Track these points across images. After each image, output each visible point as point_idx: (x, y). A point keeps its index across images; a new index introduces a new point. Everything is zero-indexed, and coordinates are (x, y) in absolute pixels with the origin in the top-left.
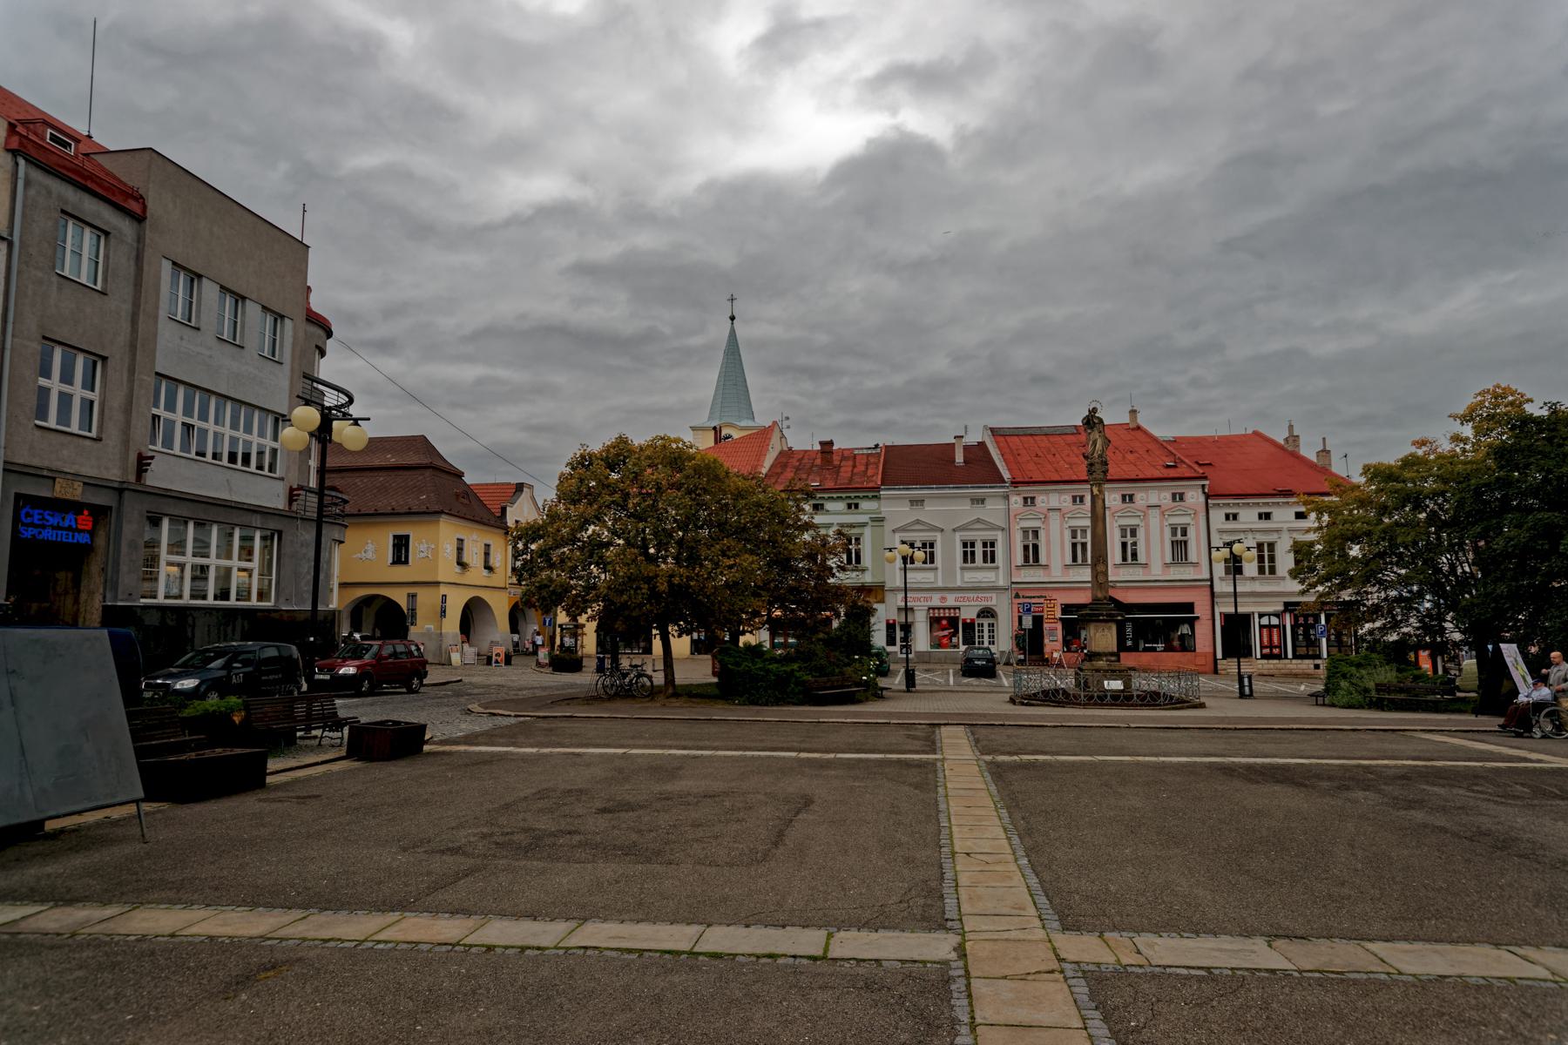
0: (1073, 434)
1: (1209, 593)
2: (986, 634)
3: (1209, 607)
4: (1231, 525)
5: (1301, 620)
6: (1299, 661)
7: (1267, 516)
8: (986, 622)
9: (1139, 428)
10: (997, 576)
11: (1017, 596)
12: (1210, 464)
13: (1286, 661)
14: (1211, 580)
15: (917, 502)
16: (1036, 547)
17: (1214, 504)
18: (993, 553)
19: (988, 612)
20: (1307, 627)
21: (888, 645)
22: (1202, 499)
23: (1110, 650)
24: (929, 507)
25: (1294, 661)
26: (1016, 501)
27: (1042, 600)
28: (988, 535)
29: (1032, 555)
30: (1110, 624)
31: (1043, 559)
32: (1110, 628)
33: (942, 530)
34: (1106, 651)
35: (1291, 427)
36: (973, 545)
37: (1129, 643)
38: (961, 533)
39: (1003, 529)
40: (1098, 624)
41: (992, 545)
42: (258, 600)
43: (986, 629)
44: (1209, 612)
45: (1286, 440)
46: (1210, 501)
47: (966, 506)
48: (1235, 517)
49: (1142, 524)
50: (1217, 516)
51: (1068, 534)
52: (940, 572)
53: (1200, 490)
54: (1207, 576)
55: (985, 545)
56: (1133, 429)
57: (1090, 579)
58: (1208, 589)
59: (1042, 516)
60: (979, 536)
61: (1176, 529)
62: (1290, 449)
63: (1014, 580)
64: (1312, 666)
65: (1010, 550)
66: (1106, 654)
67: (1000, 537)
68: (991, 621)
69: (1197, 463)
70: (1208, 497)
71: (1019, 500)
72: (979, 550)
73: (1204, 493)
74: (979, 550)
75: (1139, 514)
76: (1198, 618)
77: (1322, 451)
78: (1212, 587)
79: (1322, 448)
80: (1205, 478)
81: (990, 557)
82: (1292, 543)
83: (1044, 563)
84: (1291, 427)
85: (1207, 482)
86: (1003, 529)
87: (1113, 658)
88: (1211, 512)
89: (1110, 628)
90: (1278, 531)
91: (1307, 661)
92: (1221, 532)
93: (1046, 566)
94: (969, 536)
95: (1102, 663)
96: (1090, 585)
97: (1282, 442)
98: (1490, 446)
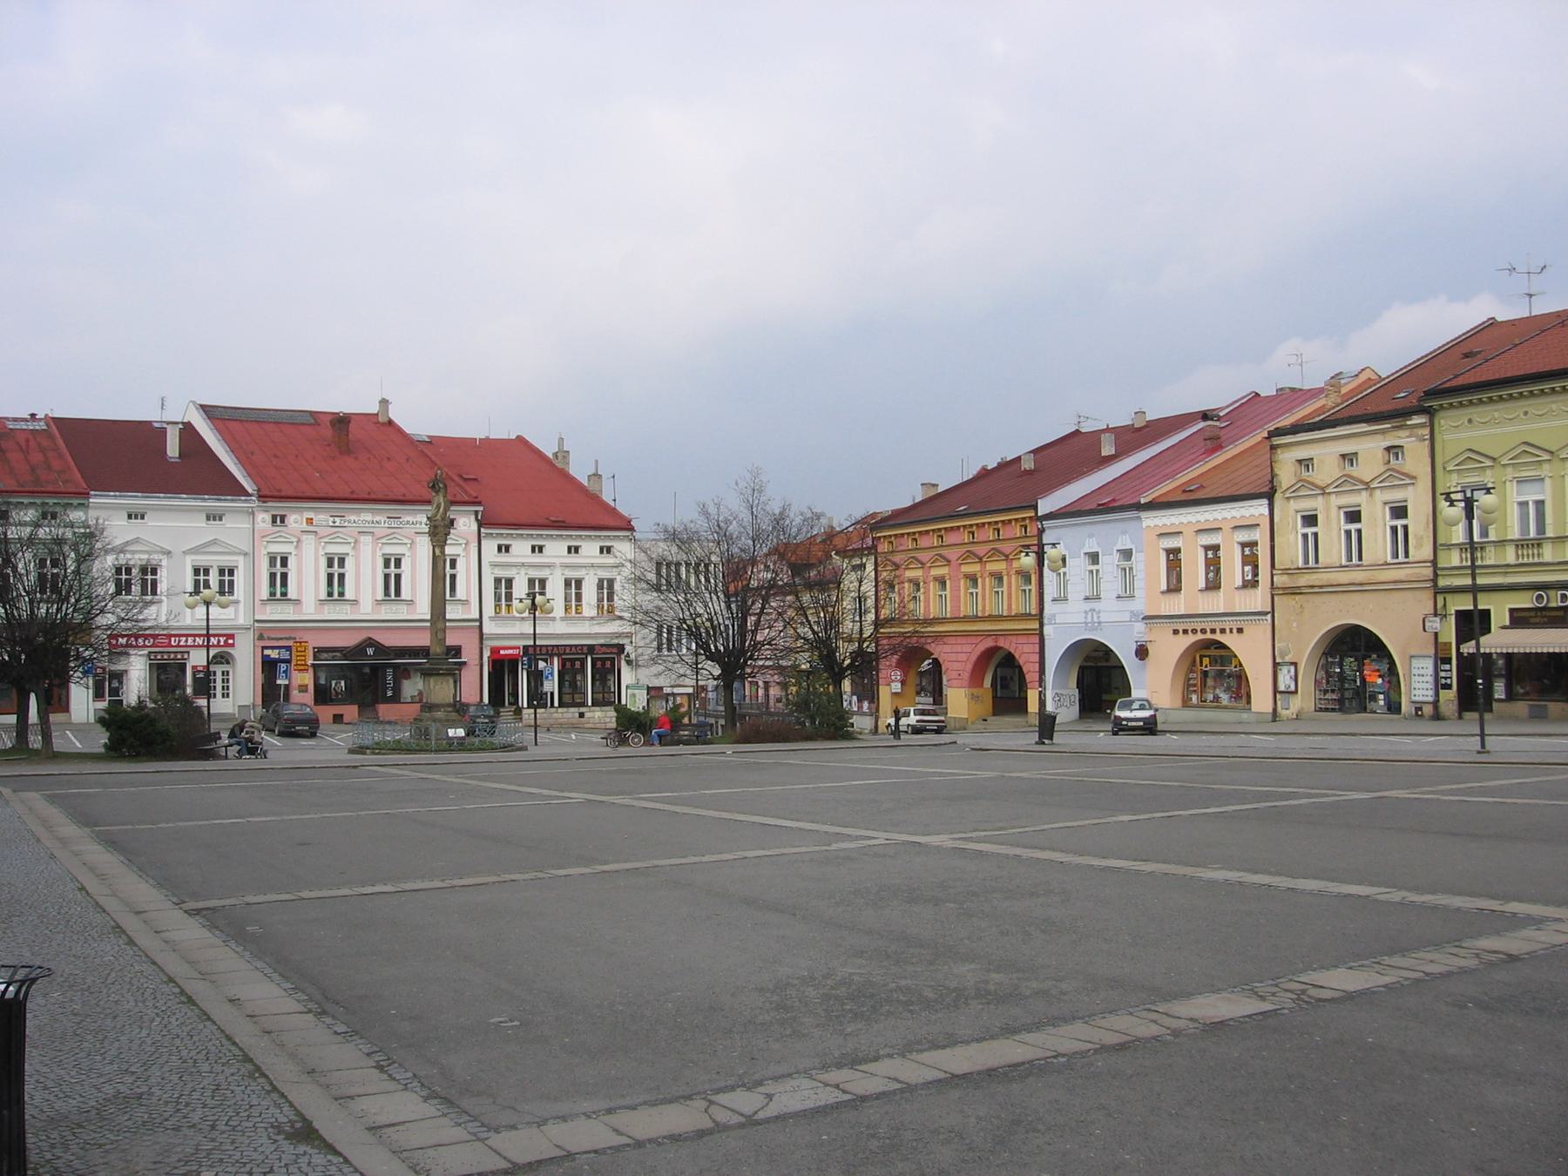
0: (311, 425)
1: (477, 636)
2: (219, 685)
3: (478, 651)
4: (504, 558)
5: (568, 665)
6: (565, 710)
7: (609, 550)
8: (218, 669)
9: (390, 422)
10: (236, 611)
11: (261, 638)
12: (475, 480)
13: (553, 710)
14: (480, 620)
15: (213, 517)
17: (486, 534)
18: (231, 583)
19: (222, 657)
20: (575, 673)
21: (315, 704)
22: (474, 526)
23: (447, 702)
24: (152, 521)
25: (560, 710)
26: (263, 519)
27: (290, 643)
28: (226, 560)
29: (279, 582)
30: (447, 678)
31: (292, 592)
32: (447, 682)
33: (170, 552)
34: (443, 702)
35: (561, 440)
36: (206, 572)
37: (390, 693)
38: (194, 557)
39: (246, 554)
40: (438, 677)
41: (231, 572)
42: (1562, 602)
43: (219, 678)
44: (478, 657)
45: (556, 455)
46: (482, 530)
47: (200, 522)
48: (507, 548)
49: (407, 554)
50: (490, 547)
51: (323, 562)
52: (241, 605)
53: (473, 517)
54: (477, 616)
55: (222, 572)
56: (383, 424)
57: (429, 617)
58: (478, 631)
59: (295, 540)
60: (214, 561)
61: (275, 558)
62: (560, 465)
63: (256, 618)
64: (577, 715)
65: (251, 582)
66: (443, 706)
67: (241, 563)
68: (225, 667)
69: (461, 476)
70: (480, 525)
71: (268, 518)
72: (214, 578)
73: (477, 519)
74: (214, 578)
75: (406, 541)
76: (465, 663)
77: (594, 475)
78: (481, 627)
79: (593, 471)
80: (479, 503)
81: (226, 588)
82: (597, 581)
83: (293, 598)
84: (561, 440)
85: (481, 508)
86: (246, 554)
87: (450, 709)
88: (482, 542)
89: (447, 682)
90: (549, 566)
91: (572, 710)
92: (494, 565)
93: (297, 602)
94: (202, 560)
95: (440, 714)
96: (428, 624)
97: (551, 456)
98: (316, 515)
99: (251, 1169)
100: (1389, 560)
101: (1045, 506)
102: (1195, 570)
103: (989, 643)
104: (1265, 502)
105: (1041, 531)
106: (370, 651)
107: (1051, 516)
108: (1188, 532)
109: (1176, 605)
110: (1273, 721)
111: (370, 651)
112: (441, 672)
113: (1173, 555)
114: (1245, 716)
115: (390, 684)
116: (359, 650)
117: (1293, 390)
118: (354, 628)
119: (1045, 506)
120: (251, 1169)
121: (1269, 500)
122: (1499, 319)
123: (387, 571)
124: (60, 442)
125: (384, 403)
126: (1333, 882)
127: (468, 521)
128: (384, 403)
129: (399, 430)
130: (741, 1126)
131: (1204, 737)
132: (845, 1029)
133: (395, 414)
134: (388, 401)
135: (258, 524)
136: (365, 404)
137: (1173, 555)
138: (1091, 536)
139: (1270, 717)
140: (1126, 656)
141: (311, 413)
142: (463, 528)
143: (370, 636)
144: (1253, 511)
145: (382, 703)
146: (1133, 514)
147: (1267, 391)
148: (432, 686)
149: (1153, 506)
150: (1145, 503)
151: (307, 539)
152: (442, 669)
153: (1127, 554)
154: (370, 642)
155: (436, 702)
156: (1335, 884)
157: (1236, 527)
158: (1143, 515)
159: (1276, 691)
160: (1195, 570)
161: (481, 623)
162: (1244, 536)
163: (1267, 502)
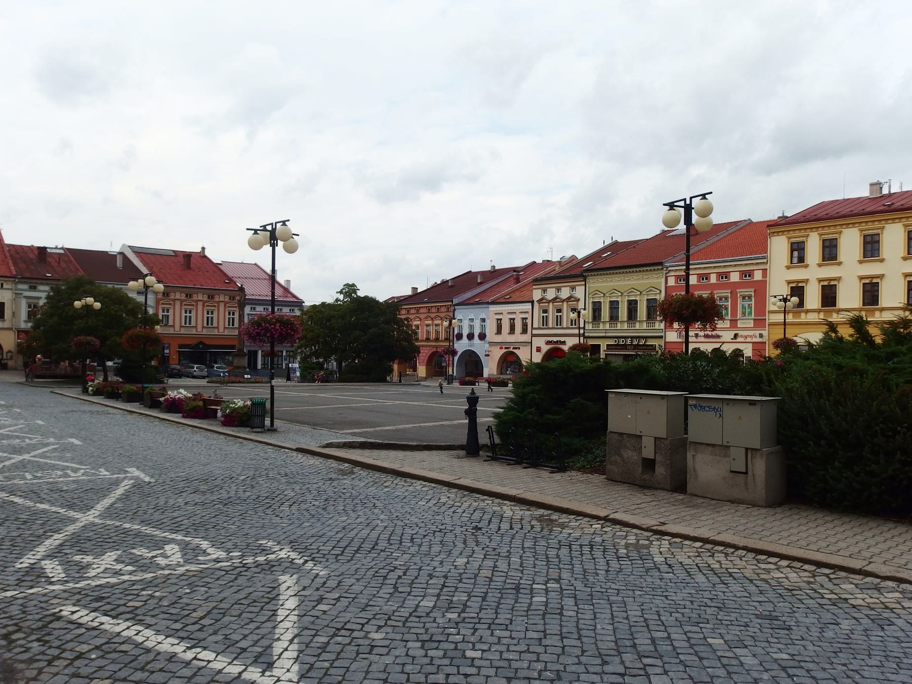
9: (205, 257)
92: (248, 315)
99: (473, 634)
100: (542, 327)
101: (455, 301)
102: (506, 327)
103: (435, 350)
104: (530, 304)
105: (454, 310)
106: (201, 346)
107: (458, 305)
109: (498, 339)
111: (201, 346)
113: (499, 321)
116: (197, 345)
117: (548, 261)
118: (222, 338)
119: (455, 301)
120: (473, 634)
122: (754, 220)
124: (72, 258)
125: (203, 249)
128: (203, 249)
129: (210, 260)
130: (375, 528)
133: (207, 253)
136: (195, 248)
137: (499, 321)
140: (482, 356)
141: (173, 251)
144: (526, 307)
145: (427, 369)
146: (487, 306)
147: (539, 261)
149: (494, 303)
153: (483, 320)
154: (201, 343)
157: (495, 314)
158: (490, 306)
160: (506, 327)
162: (524, 316)
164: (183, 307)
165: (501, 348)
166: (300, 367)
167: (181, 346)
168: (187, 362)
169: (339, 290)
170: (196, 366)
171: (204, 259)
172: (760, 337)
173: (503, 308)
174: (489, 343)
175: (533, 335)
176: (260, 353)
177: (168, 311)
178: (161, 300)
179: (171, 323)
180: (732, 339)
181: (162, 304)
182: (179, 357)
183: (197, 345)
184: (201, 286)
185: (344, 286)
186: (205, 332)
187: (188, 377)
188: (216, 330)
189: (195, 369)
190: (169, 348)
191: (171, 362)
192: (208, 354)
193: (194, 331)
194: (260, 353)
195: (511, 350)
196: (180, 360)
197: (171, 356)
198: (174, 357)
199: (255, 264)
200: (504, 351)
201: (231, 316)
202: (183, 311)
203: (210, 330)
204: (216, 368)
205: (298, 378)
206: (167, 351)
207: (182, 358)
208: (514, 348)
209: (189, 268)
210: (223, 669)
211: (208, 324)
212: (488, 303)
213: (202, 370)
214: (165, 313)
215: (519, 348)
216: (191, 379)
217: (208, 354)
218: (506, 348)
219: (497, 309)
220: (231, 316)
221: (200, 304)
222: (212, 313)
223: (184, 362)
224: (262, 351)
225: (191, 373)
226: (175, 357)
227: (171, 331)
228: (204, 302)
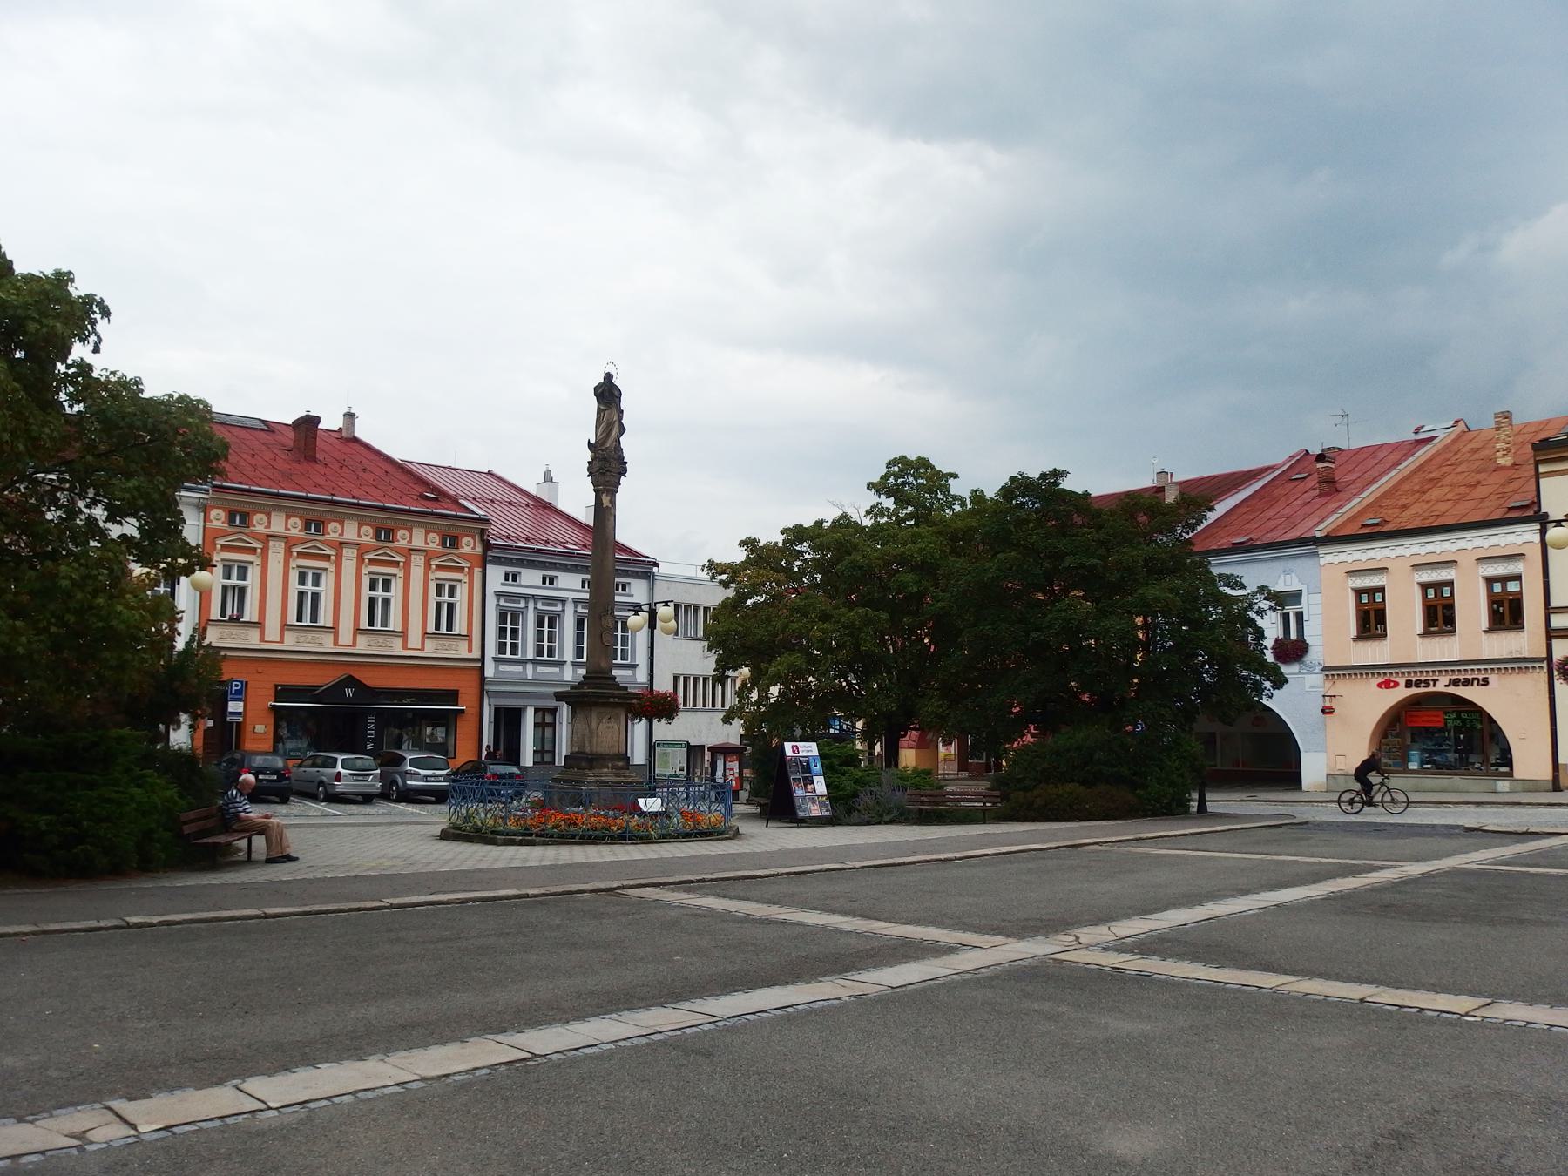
9: (356, 440)
14: (482, 659)
16: (451, 607)
92: (499, 595)
106: (349, 692)
108: (1466, 561)
110: (1555, 790)
111: (349, 692)
112: (611, 700)
114: (1503, 785)
115: (371, 734)
116: (336, 690)
121: (1541, 524)
123: (373, 594)
125: (350, 416)
126: (356, 876)
127: (472, 541)
128: (350, 416)
131: (1489, 810)
132: (506, 1070)
133: (361, 432)
134: (354, 415)
135: (211, 521)
138: (1286, 572)
139: (1550, 786)
142: (466, 548)
143: (352, 674)
146: (1311, 549)
148: (594, 725)
149: (1331, 540)
150: (1322, 537)
151: (274, 546)
152: (614, 696)
154: (351, 681)
155: (599, 750)
156: (353, 874)
158: (1322, 550)
159: (384, 796)
161: (483, 663)
163: (1539, 527)
164: (293, 564)
165: (1387, 684)
166: (822, 756)
167: (282, 692)
168: (303, 744)
169: (876, 479)
170: (340, 758)
171: (356, 446)
172: (1407, 687)
173: (1386, 552)
174: (1326, 669)
175: (1551, 634)
176: (530, 713)
177: (243, 575)
178: (221, 534)
179: (250, 613)
180: (1446, 686)
181: (225, 548)
182: (276, 727)
183: (338, 687)
184: (354, 497)
185: (889, 465)
186: (363, 645)
187: (313, 797)
188: (398, 642)
189: (339, 768)
190: (240, 694)
191: (249, 745)
192: (371, 720)
193: (327, 644)
194: (530, 713)
195: (1440, 687)
196: (277, 739)
197: (249, 728)
198: (260, 728)
199: (490, 473)
200: (1401, 693)
201: (446, 598)
202: (294, 577)
203: (381, 639)
204: (414, 763)
205: (822, 804)
206: (235, 706)
207: (284, 732)
208: (1455, 683)
209: (312, 459)
210: (109, 320)
211: (371, 623)
212: (1314, 541)
213: (362, 773)
214: (234, 581)
215: (1486, 682)
216: (323, 807)
217: (371, 720)
218: (1409, 684)
219: (1357, 556)
220: (446, 598)
221: (350, 555)
222: (387, 586)
223: (290, 745)
224: (536, 711)
225: (321, 783)
226: (262, 727)
227: (252, 639)
228: (362, 550)
